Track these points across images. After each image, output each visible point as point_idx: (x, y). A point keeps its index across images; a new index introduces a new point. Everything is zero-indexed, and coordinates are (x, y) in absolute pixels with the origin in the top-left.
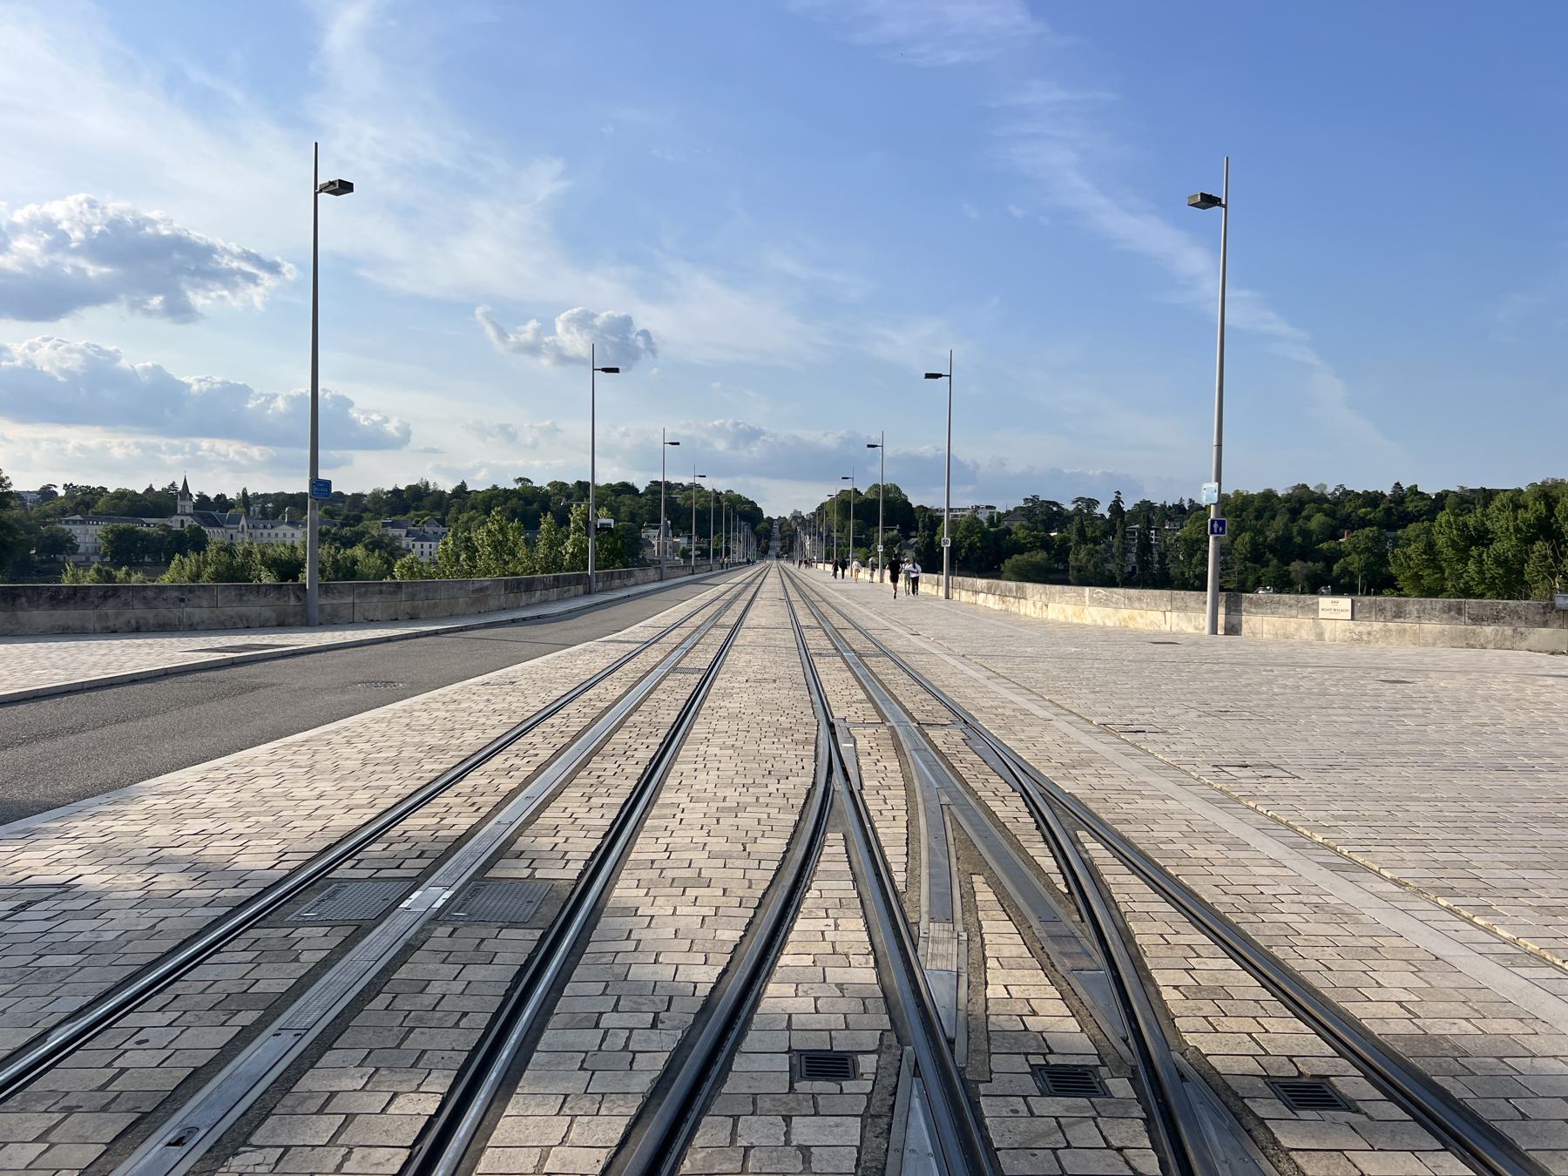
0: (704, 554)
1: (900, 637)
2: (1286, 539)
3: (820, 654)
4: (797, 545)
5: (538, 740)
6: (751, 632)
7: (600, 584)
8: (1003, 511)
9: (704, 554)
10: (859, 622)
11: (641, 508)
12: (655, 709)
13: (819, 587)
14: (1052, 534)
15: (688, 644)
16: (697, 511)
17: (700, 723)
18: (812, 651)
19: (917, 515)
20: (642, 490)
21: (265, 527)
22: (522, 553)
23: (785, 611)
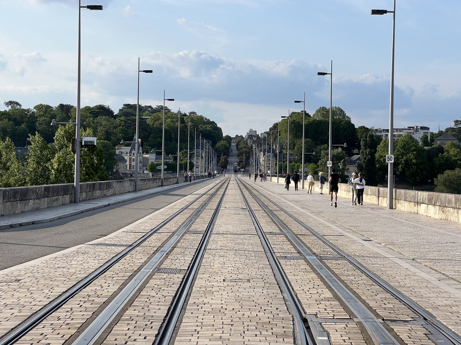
0: (171, 168)
1: (354, 242)
3: (285, 257)
4: (252, 161)
5: (48, 331)
6: (221, 237)
7: (84, 194)
8: (436, 131)
9: (171, 168)
10: (316, 229)
11: (115, 128)
12: (147, 304)
13: (276, 198)
15: (167, 248)
16: (166, 130)
17: (188, 317)
18: (278, 255)
19: (359, 135)
20: (116, 112)
22: (14, 166)
23: (249, 219)
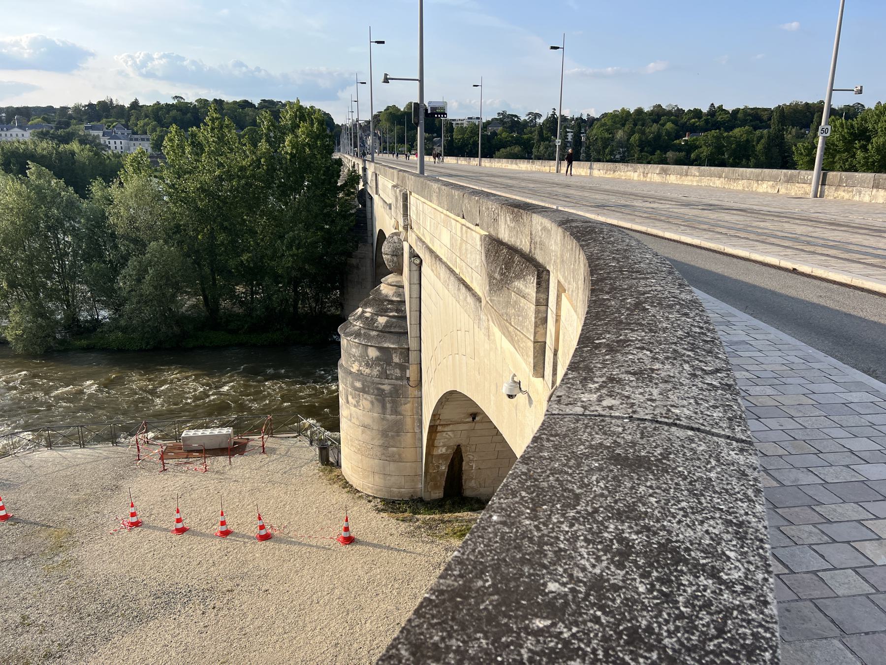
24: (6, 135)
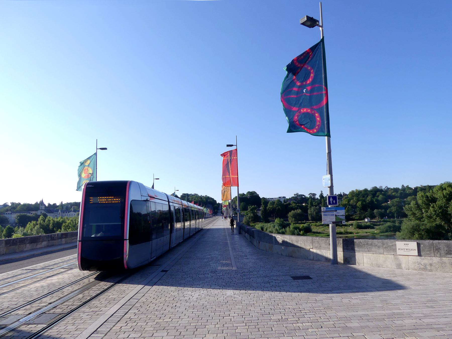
2: (372, 202)
14: (303, 204)
21: (66, 213)
24: (67, 215)
